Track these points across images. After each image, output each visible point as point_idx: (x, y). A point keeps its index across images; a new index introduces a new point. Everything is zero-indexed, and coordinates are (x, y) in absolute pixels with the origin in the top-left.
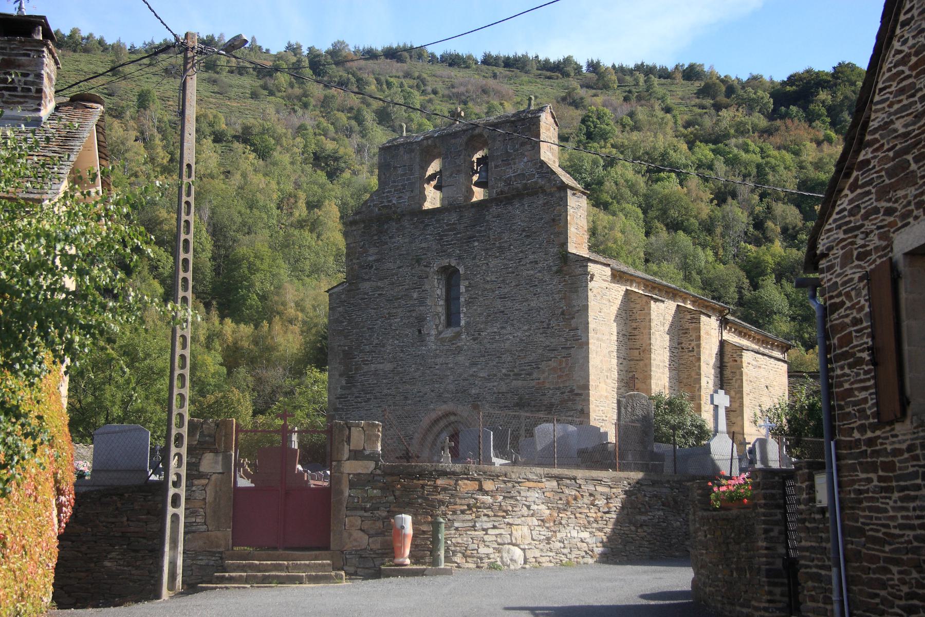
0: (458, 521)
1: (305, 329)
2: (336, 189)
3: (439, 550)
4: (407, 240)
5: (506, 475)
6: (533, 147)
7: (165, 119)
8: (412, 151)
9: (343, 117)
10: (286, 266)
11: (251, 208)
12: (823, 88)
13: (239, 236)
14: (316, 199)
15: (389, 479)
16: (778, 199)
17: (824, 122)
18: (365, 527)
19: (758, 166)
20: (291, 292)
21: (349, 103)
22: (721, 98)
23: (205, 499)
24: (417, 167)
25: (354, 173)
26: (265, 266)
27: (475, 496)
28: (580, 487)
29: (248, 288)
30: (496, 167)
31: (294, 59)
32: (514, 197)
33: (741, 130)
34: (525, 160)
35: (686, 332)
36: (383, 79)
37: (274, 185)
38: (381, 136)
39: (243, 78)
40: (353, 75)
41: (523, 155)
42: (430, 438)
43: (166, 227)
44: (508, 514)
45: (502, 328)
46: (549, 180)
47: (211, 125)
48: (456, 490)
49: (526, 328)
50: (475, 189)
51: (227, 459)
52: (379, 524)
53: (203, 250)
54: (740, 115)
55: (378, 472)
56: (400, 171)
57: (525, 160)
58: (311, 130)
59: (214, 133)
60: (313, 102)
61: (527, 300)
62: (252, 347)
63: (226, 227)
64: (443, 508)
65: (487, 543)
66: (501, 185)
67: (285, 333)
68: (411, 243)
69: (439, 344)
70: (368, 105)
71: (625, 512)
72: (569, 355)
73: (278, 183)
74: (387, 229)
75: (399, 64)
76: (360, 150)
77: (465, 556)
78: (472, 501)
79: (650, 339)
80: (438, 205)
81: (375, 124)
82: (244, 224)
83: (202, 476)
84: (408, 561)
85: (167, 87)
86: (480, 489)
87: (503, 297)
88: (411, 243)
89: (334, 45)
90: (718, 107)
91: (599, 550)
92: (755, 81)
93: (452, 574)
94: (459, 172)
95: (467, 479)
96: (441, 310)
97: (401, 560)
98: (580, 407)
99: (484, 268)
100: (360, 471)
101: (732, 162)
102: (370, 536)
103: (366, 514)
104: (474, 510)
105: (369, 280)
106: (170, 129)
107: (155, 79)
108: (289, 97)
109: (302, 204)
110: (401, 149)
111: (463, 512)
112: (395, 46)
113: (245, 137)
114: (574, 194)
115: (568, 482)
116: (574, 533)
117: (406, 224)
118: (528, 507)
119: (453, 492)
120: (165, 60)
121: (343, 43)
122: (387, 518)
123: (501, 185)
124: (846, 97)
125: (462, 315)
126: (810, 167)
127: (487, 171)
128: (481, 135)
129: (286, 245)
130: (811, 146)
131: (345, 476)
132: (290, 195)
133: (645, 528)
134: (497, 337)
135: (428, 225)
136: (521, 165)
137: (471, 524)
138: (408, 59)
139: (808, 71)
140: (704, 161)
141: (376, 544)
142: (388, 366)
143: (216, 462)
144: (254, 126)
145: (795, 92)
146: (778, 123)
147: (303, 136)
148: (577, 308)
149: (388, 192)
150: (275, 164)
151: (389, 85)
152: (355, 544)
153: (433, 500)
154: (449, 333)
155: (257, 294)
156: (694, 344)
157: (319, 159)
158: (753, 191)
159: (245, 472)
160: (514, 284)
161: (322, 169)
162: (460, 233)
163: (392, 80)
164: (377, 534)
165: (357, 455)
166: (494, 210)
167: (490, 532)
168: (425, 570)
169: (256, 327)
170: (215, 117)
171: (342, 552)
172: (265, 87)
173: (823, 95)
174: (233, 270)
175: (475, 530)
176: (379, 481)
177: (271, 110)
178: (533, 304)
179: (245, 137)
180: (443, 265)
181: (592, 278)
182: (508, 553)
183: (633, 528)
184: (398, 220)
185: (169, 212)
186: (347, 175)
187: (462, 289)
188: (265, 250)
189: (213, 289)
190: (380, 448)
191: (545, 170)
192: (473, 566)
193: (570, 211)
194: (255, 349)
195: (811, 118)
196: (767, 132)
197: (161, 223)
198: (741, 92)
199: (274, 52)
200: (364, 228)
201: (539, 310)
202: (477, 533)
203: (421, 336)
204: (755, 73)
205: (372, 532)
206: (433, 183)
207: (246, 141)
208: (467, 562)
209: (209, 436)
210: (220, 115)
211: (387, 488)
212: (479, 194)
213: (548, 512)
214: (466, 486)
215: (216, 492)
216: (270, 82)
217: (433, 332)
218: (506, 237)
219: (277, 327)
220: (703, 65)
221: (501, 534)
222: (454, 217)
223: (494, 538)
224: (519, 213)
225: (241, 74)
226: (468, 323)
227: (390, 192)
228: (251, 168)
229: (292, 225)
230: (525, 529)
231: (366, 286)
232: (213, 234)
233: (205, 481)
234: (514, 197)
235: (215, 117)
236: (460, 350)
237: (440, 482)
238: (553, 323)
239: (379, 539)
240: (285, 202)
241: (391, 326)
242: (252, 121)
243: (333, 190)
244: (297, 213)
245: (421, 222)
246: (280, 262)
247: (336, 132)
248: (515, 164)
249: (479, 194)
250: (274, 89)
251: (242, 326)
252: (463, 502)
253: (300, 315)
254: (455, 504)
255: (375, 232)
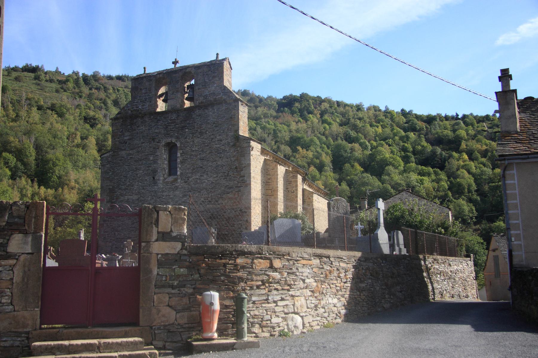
0: (255, 295)
1: (79, 192)
2: (94, 132)
3: (243, 323)
5: (289, 254)
7: (14, 98)
9: (98, 102)
10: (71, 164)
11: (54, 138)
12: (297, 102)
13: (49, 150)
14: (85, 136)
15: (194, 258)
16: (282, 144)
17: (297, 115)
18: (173, 304)
19: (274, 130)
20: (73, 175)
21: (100, 97)
22: (257, 103)
23: (12, 279)
25: (102, 125)
26: (60, 164)
27: (268, 273)
28: (332, 264)
29: (52, 173)
30: (199, 89)
31: (76, 77)
33: (266, 116)
34: (215, 85)
35: (290, 182)
36: (116, 88)
37: (66, 129)
38: (114, 111)
39: (52, 84)
40: (102, 85)
41: (214, 83)
43: (13, 145)
44: (291, 288)
45: (201, 176)
46: (229, 96)
47: (36, 102)
48: (252, 268)
49: (215, 176)
50: (186, 102)
51: (37, 240)
52: (186, 300)
53: (31, 156)
54: (265, 110)
55: (185, 252)
56: (144, 91)
57: (215, 85)
58: (83, 107)
59: (38, 106)
60: (84, 95)
61: (215, 161)
62: (54, 199)
63: (42, 146)
64: (242, 284)
65: (277, 314)
66: (201, 99)
67: (70, 193)
68: (149, 129)
69: (165, 184)
71: (354, 282)
72: (240, 191)
73: (68, 128)
76: (105, 116)
77: (261, 327)
78: (265, 278)
79: (277, 184)
80: (164, 110)
82: (51, 145)
84: (216, 335)
85: (15, 85)
86: (271, 267)
87: (202, 159)
88: (149, 129)
89: (94, 73)
90: (256, 107)
91: (343, 312)
92: (270, 98)
93: (259, 347)
94: (177, 92)
95: (261, 258)
96: (166, 166)
97: (210, 334)
98: (246, 219)
100: (167, 251)
101: (263, 128)
102: (178, 312)
103: (173, 291)
104: (267, 285)
105: (125, 150)
106: (16, 103)
107: (10, 82)
108: (73, 93)
109: (78, 137)
110: (144, 79)
111: (258, 287)
112: (121, 75)
113: (53, 108)
114: (242, 105)
115: (325, 259)
116: (330, 301)
117: (147, 119)
118: (304, 281)
119: (249, 268)
120: (14, 74)
121: (98, 72)
122: (193, 294)
124: (305, 106)
125: (178, 169)
126: (294, 131)
127: (193, 92)
128: (190, 72)
129: (71, 155)
130: (294, 123)
131: (154, 256)
132: (73, 134)
133: (364, 293)
134: (198, 181)
136: (212, 88)
137: (265, 298)
139: (291, 95)
141: (183, 319)
142: (135, 197)
143: (26, 243)
144: (57, 103)
145: (286, 103)
146: (280, 114)
147: (79, 109)
148: (243, 166)
150: (67, 120)
151: (118, 90)
152: (163, 319)
153: (234, 278)
154: (171, 179)
155: (57, 176)
156: (294, 189)
157: (86, 119)
158: (272, 140)
159: (51, 255)
160: (208, 152)
161: (88, 123)
164: (184, 310)
165: (165, 236)
166: (197, 112)
167: (280, 303)
168: (234, 344)
169: (56, 191)
170: (38, 99)
171: (151, 328)
172: (62, 88)
173: (297, 104)
174: (46, 165)
175: (268, 303)
176: (186, 261)
177: (65, 97)
178: (219, 163)
179: (53, 108)
181: (252, 149)
182: (292, 321)
183: (358, 293)
185: (14, 138)
186: (99, 126)
187: (179, 155)
188: (61, 156)
189: (36, 173)
190: (186, 231)
192: (267, 335)
193: (240, 113)
194: (55, 200)
195: (293, 113)
196: (276, 118)
197: (11, 143)
198: (264, 101)
199: (66, 74)
200: (123, 121)
201: (222, 166)
202: (270, 305)
203: (154, 181)
204: (269, 95)
205: (179, 308)
206: (162, 99)
207: (52, 110)
208: (263, 331)
209: (19, 217)
210: (41, 98)
211: (193, 267)
212: (187, 104)
213: (315, 284)
214: (260, 264)
215: (25, 272)
216: (65, 86)
217: (162, 178)
218: (204, 126)
219: (66, 190)
221: (287, 305)
222: (174, 116)
223: (282, 309)
225: (51, 82)
226: (181, 174)
228: (55, 121)
229: (73, 146)
230: (303, 299)
231: (123, 153)
232: (36, 149)
233: (12, 262)
235: (38, 99)
236: (177, 188)
237: (240, 261)
238: (231, 173)
239: (186, 314)
240: (71, 137)
241: (137, 175)
242: (56, 101)
243: (93, 132)
244: (76, 141)
246: (68, 162)
247: (95, 108)
248: (209, 87)
249: (187, 104)
250: (66, 89)
251: (49, 190)
252: (259, 278)
253: (77, 185)
254: (252, 281)
255: (129, 124)
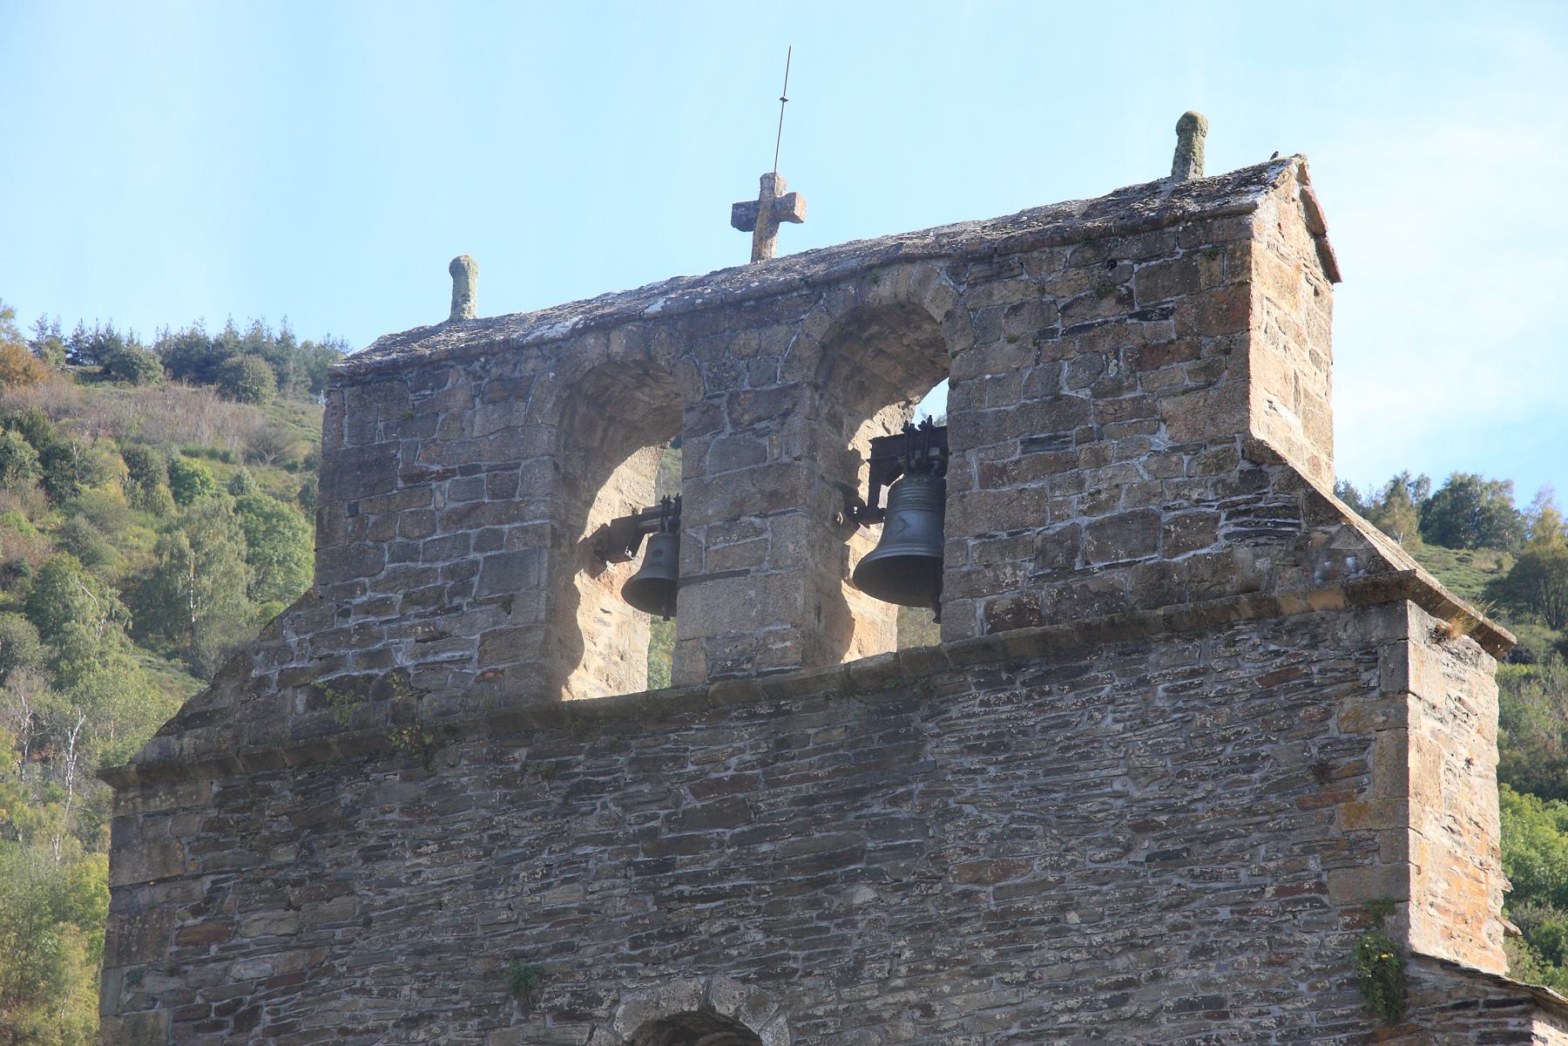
4: (465, 870)
6: (1210, 374)
8: (514, 390)
24: (539, 478)
30: (992, 475)
32: (1091, 638)
34: (1162, 439)
36: (157, 458)
41: (1147, 414)
46: (1300, 553)
56: (443, 498)
57: (1162, 439)
66: (1018, 573)
68: (485, 883)
70: (90, 559)
74: (353, 810)
75: (230, 407)
80: (637, 683)
81: (118, 635)
88: (485, 883)
94: (777, 501)
99: (907, 1029)
110: (456, 378)
114: (1439, 636)
123: (1018, 573)
127: (936, 504)
135: (588, 789)
136: (1132, 471)
138: (269, 389)
140: (1541, 869)
149: (368, 609)
151: (182, 484)
162: (772, 834)
163: (196, 464)
166: (978, 710)
180: (669, 1008)
184: (422, 758)
191: (1272, 497)
200: (222, 800)
206: (622, 571)
212: (875, 628)
220: (1507, 485)
222: (737, 749)
224: (1120, 729)
227: (380, 606)
234: (1091, 638)
245: (557, 772)
248: (1099, 460)
249: (875, 628)
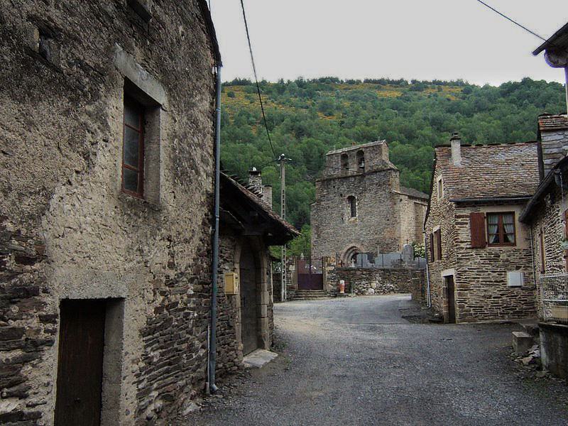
42: (347, 256)
83: (289, 271)
154: (353, 219)
226: (359, 216)
237: (470, 246)
